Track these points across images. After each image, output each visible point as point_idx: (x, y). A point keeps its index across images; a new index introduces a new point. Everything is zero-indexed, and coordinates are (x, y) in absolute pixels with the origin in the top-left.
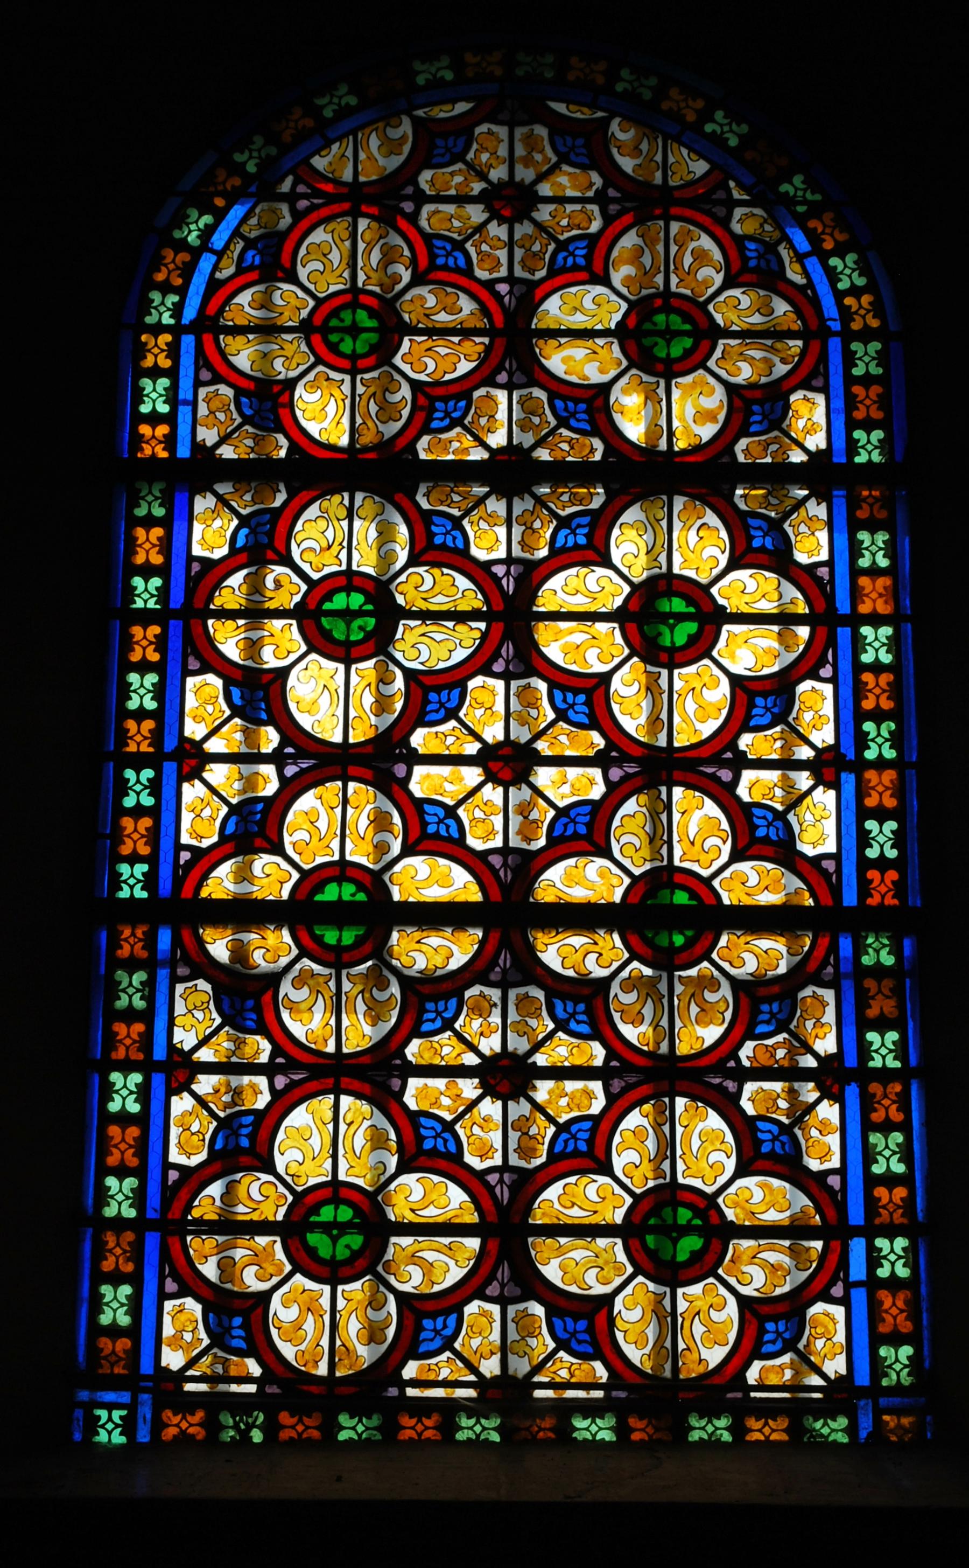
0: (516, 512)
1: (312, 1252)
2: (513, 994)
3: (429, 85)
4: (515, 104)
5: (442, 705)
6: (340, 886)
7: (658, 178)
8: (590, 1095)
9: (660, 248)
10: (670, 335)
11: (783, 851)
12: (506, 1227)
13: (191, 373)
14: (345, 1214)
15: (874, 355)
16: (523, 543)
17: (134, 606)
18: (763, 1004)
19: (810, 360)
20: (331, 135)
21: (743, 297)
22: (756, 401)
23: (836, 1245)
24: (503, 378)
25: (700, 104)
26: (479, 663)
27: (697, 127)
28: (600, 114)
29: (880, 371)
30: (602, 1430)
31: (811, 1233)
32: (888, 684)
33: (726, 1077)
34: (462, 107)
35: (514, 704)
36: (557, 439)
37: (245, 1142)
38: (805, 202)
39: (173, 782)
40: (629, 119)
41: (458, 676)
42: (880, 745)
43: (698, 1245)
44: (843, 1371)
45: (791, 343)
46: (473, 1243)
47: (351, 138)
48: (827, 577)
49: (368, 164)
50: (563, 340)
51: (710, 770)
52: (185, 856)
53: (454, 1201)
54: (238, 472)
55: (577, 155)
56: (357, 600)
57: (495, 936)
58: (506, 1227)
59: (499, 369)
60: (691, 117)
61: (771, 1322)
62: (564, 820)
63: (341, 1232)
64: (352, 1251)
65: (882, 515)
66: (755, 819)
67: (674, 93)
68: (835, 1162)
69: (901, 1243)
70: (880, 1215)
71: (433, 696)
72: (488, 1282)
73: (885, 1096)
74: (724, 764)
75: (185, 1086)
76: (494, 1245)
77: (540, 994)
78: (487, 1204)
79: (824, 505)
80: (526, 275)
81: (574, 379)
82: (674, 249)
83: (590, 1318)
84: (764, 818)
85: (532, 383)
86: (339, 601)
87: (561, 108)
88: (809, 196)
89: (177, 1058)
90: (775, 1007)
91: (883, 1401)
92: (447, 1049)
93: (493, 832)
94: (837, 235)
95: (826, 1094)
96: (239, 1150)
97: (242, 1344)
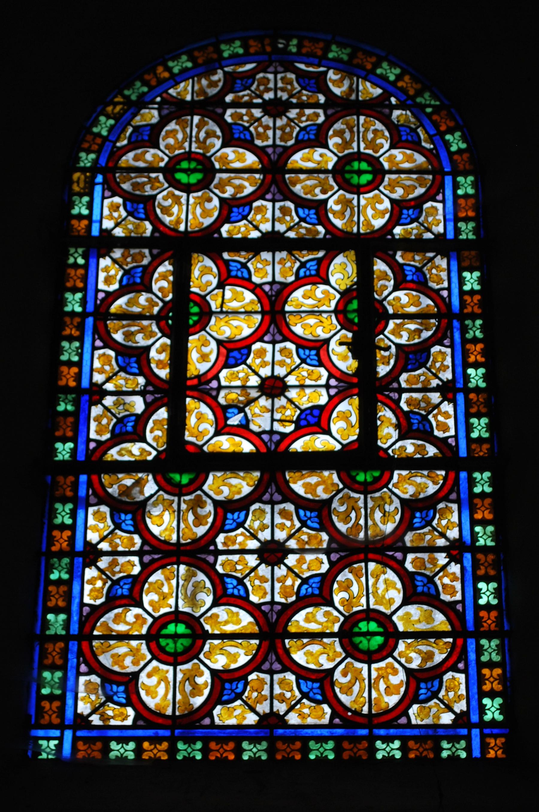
0: (277, 259)
1: (162, 649)
2: (279, 76)
3: (231, 57)
4: (276, 60)
5: (233, 691)
6: (176, 632)
7: (355, 230)
8: (317, 115)
9: (363, 579)
10: (360, 173)
11: (425, 434)
12: (272, 632)
13: (100, 194)
14: (193, 165)
15: (490, 535)
16: (282, 139)
17: (57, 459)
18: (417, 510)
19: (450, 482)
20: (178, 80)
21: (415, 611)
22: (410, 353)
23: (438, 177)
24: (269, 196)
25: (374, 59)
26: (258, 335)
27: (372, 72)
28: (322, 69)
29: (493, 544)
30: (328, 751)
31: (427, 172)
32: (497, 646)
33: (396, 552)
34: (249, 67)
35: (278, 214)
36: (300, 370)
37: (138, 280)
38: (430, 106)
39: (86, 406)
40: (337, 70)
41: (248, 200)
42: (476, 376)
43: (381, 647)
44: (465, 709)
45: (426, 176)
46: (255, 642)
47: (191, 81)
48: (454, 444)
49: (186, 530)
50: (305, 641)
51: (391, 553)
52: (92, 445)
53: (251, 159)
54: (127, 243)
55: (311, 360)
56: (181, 629)
57: (266, 477)
58: (272, 632)
59: (267, 332)
60: (369, 66)
61: (422, 683)
62: (303, 132)
63: (179, 640)
64: (185, 647)
65: (492, 573)
66: (416, 582)
67: (360, 55)
68: (452, 432)
69: (495, 643)
70: (483, 626)
71: (227, 686)
72: (263, 662)
73: (489, 618)
74: (397, 550)
75: (99, 402)
76: (266, 644)
77: (292, 206)
78: (266, 159)
79: (451, 405)
80: (282, 144)
81: (310, 337)
82: (371, 581)
83: (318, 349)
84: (411, 271)
85: (285, 339)
86: (171, 628)
87: (302, 66)
88: (433, 102)
89: (94, 388)
90: (411, 212)
91: (487, 731)
92: (240, 538)
93: (265, 593)
94: (448, 122)
95: (445, 398)
96: (135, 283)
97: (136, 371)
